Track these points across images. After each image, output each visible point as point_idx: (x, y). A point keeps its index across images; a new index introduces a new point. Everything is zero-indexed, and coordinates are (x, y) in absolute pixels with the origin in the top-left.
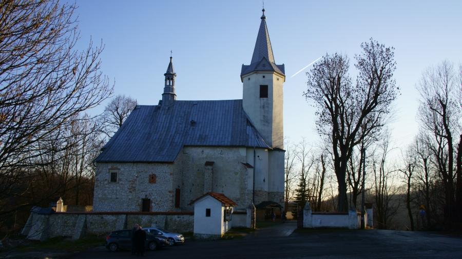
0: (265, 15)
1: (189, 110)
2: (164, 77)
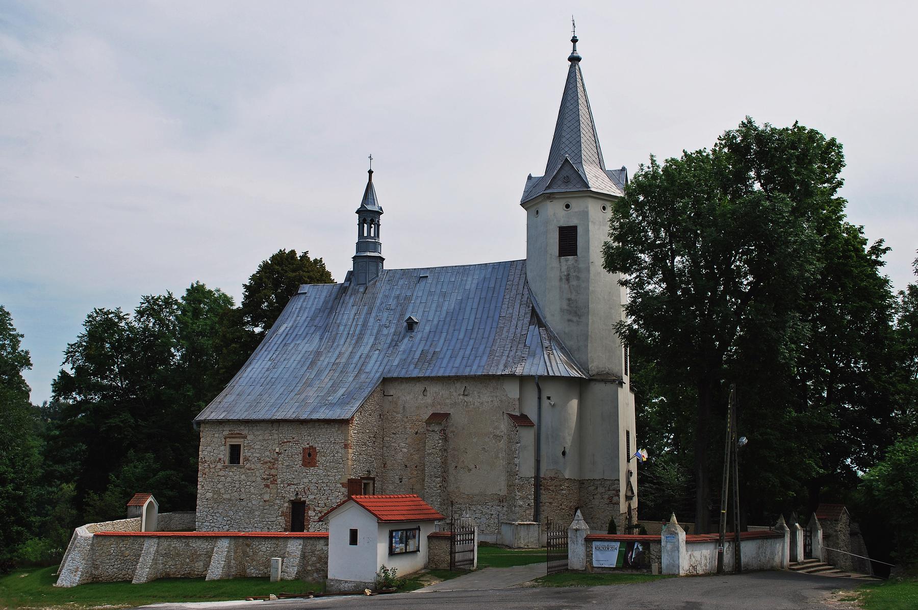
0: (580, 52)
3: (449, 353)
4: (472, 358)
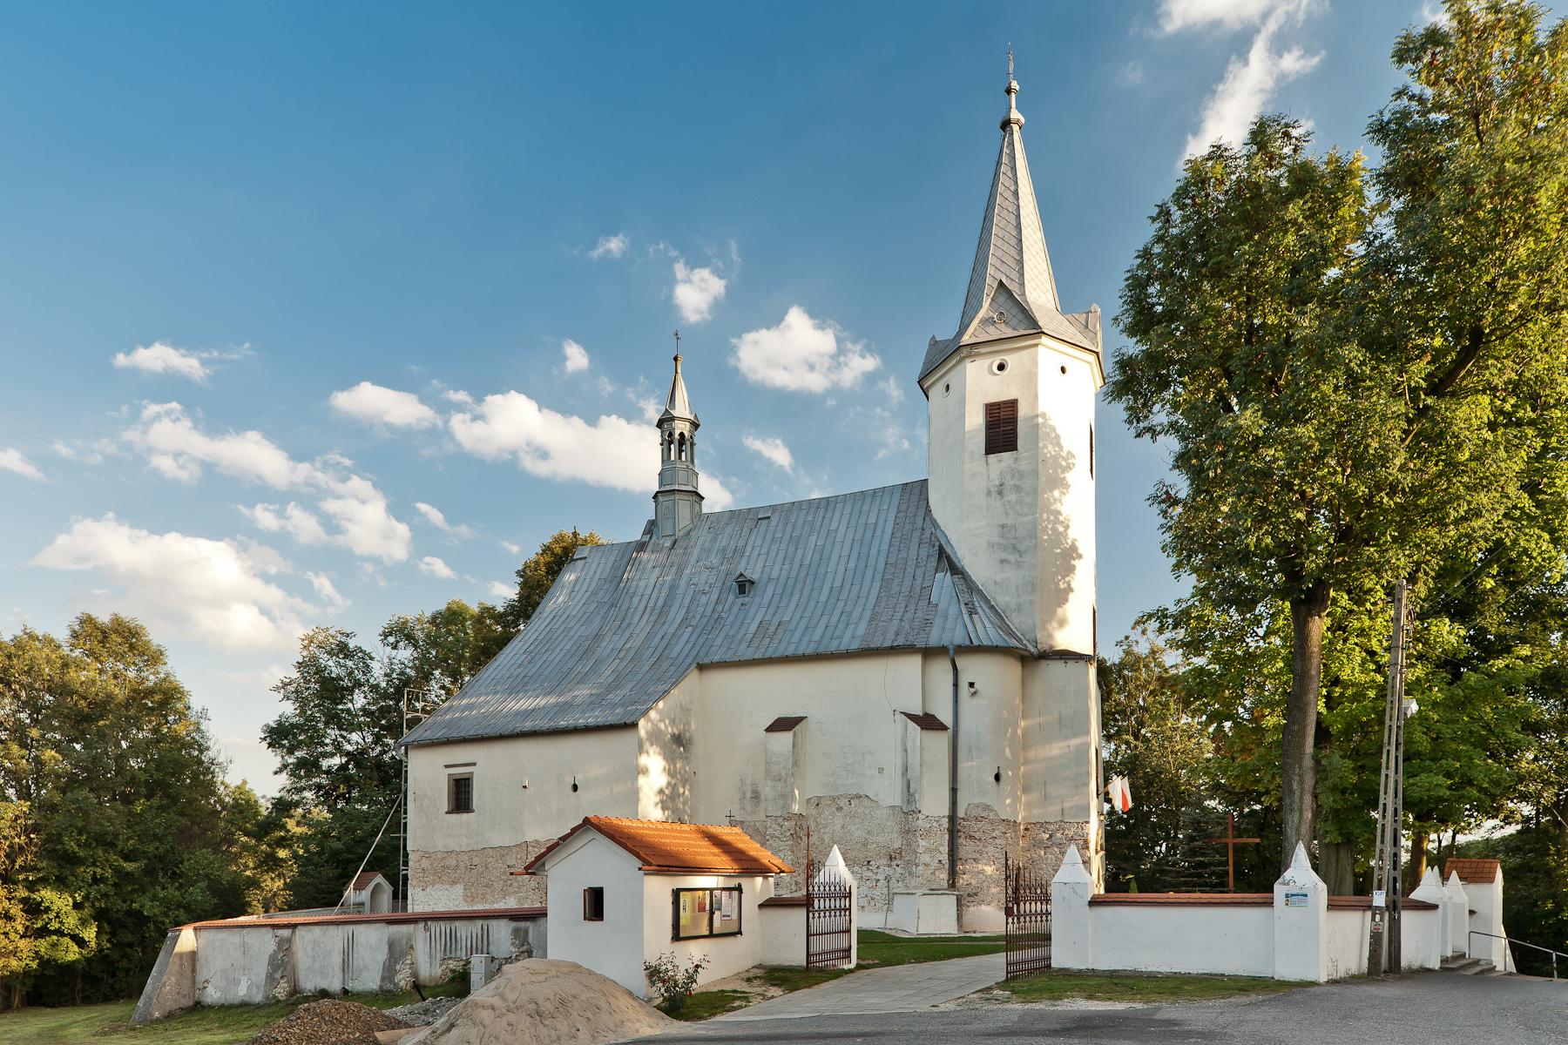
1: (741, 543)
3: (804, 622)
4: (841, 626)
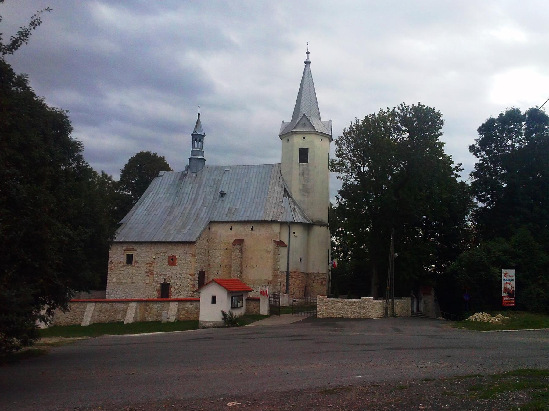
0: (310, 59)
1: (220, 178)
2: (140, 152)
